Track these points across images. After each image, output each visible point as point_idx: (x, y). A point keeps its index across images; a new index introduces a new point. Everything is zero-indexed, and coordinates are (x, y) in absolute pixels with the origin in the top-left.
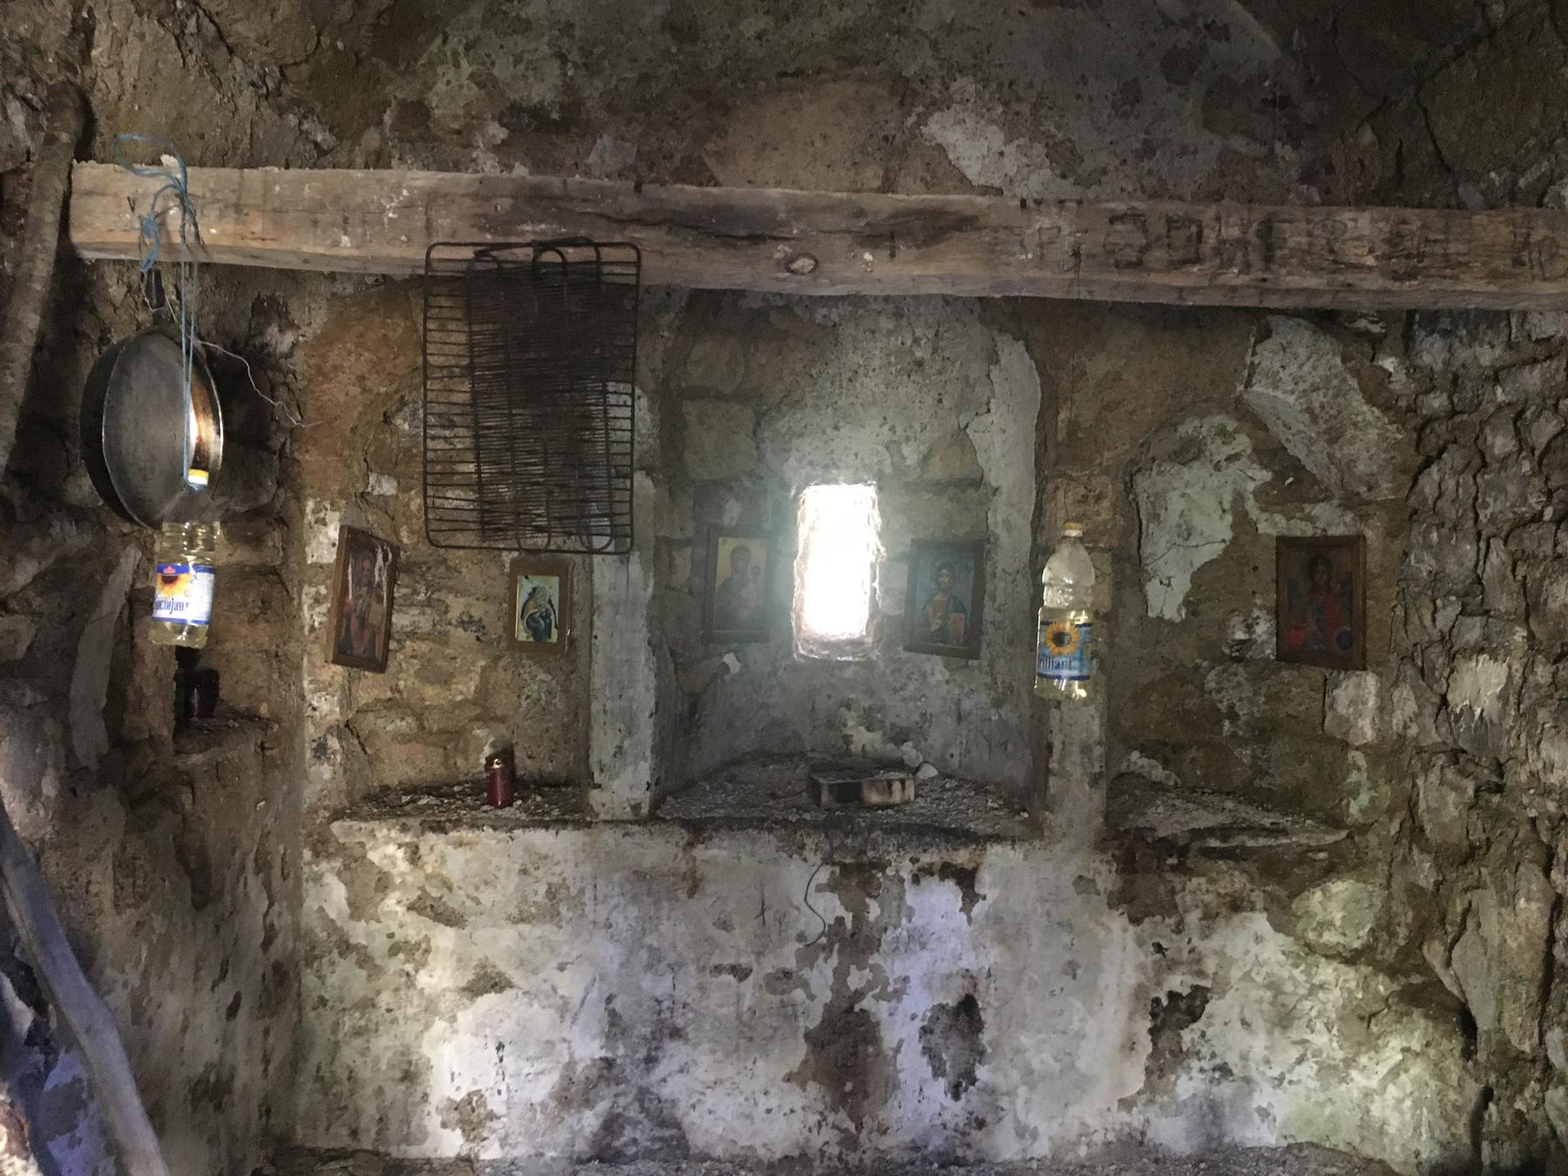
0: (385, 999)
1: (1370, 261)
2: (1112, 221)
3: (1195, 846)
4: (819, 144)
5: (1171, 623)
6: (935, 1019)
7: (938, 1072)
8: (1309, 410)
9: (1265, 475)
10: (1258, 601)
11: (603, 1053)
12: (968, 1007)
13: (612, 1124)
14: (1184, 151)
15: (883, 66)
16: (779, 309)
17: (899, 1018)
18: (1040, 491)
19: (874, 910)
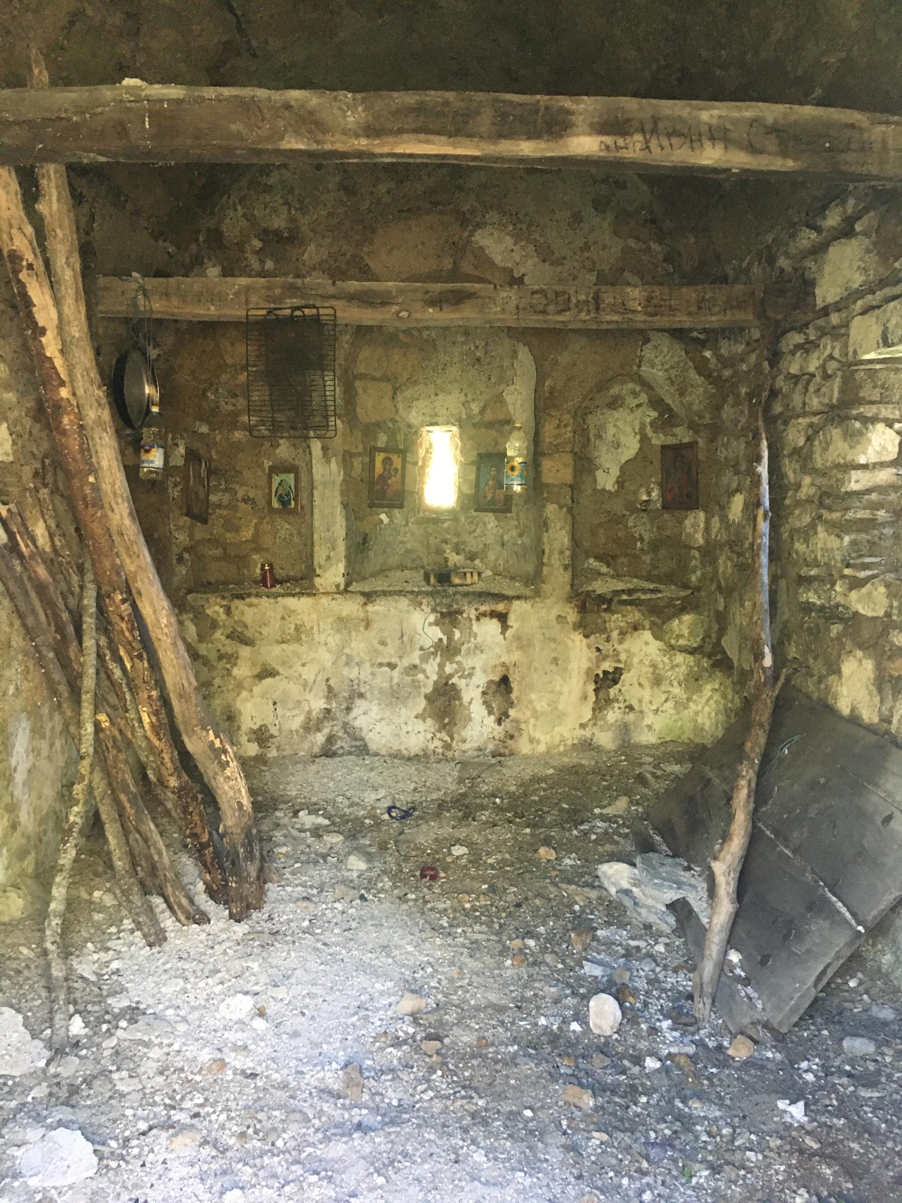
0: (217, 681)
1: (639, 309)
2: (533, 293)
3: (616, 599)
4: (420, 247)
5: (609, 492)
6: (488, 687)
7: (490, 713)
8: (670, 379)
9: (654, 414)
10: (653, 480)
11: (326, 706)
12: (504, 683)
13: (330, 739)
14: (604, 247)
15: (452, 206)
16: (404, 332)
17: (471, 687)
18: (537, 424)
19: (457, 635)
